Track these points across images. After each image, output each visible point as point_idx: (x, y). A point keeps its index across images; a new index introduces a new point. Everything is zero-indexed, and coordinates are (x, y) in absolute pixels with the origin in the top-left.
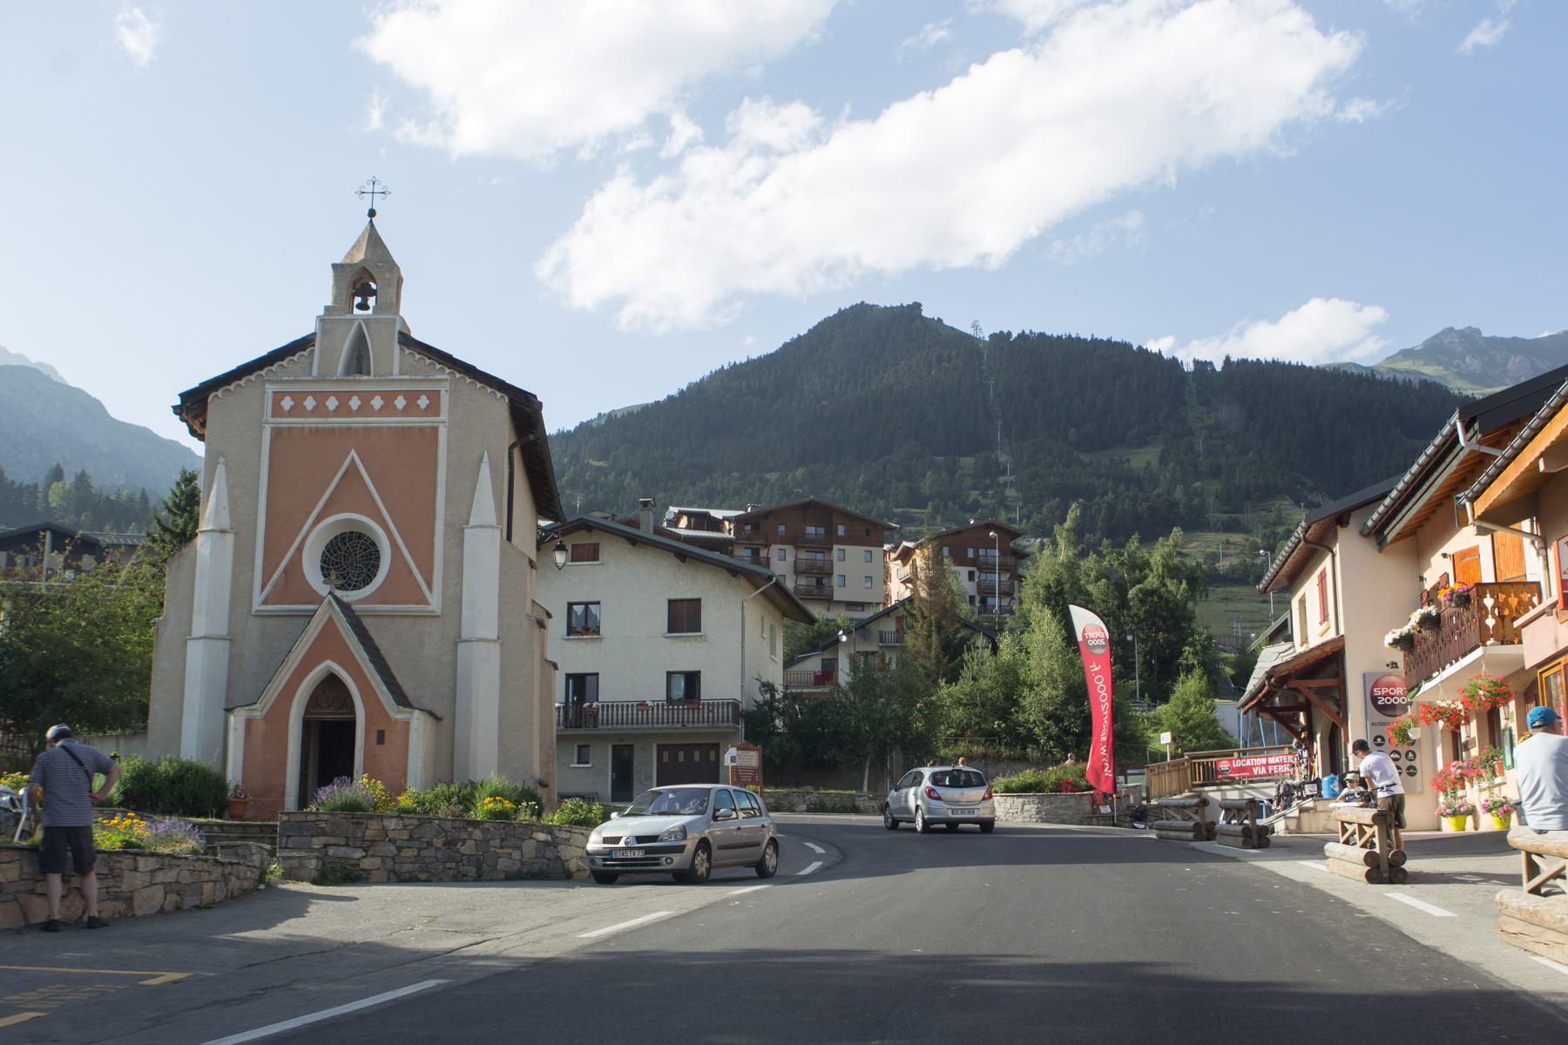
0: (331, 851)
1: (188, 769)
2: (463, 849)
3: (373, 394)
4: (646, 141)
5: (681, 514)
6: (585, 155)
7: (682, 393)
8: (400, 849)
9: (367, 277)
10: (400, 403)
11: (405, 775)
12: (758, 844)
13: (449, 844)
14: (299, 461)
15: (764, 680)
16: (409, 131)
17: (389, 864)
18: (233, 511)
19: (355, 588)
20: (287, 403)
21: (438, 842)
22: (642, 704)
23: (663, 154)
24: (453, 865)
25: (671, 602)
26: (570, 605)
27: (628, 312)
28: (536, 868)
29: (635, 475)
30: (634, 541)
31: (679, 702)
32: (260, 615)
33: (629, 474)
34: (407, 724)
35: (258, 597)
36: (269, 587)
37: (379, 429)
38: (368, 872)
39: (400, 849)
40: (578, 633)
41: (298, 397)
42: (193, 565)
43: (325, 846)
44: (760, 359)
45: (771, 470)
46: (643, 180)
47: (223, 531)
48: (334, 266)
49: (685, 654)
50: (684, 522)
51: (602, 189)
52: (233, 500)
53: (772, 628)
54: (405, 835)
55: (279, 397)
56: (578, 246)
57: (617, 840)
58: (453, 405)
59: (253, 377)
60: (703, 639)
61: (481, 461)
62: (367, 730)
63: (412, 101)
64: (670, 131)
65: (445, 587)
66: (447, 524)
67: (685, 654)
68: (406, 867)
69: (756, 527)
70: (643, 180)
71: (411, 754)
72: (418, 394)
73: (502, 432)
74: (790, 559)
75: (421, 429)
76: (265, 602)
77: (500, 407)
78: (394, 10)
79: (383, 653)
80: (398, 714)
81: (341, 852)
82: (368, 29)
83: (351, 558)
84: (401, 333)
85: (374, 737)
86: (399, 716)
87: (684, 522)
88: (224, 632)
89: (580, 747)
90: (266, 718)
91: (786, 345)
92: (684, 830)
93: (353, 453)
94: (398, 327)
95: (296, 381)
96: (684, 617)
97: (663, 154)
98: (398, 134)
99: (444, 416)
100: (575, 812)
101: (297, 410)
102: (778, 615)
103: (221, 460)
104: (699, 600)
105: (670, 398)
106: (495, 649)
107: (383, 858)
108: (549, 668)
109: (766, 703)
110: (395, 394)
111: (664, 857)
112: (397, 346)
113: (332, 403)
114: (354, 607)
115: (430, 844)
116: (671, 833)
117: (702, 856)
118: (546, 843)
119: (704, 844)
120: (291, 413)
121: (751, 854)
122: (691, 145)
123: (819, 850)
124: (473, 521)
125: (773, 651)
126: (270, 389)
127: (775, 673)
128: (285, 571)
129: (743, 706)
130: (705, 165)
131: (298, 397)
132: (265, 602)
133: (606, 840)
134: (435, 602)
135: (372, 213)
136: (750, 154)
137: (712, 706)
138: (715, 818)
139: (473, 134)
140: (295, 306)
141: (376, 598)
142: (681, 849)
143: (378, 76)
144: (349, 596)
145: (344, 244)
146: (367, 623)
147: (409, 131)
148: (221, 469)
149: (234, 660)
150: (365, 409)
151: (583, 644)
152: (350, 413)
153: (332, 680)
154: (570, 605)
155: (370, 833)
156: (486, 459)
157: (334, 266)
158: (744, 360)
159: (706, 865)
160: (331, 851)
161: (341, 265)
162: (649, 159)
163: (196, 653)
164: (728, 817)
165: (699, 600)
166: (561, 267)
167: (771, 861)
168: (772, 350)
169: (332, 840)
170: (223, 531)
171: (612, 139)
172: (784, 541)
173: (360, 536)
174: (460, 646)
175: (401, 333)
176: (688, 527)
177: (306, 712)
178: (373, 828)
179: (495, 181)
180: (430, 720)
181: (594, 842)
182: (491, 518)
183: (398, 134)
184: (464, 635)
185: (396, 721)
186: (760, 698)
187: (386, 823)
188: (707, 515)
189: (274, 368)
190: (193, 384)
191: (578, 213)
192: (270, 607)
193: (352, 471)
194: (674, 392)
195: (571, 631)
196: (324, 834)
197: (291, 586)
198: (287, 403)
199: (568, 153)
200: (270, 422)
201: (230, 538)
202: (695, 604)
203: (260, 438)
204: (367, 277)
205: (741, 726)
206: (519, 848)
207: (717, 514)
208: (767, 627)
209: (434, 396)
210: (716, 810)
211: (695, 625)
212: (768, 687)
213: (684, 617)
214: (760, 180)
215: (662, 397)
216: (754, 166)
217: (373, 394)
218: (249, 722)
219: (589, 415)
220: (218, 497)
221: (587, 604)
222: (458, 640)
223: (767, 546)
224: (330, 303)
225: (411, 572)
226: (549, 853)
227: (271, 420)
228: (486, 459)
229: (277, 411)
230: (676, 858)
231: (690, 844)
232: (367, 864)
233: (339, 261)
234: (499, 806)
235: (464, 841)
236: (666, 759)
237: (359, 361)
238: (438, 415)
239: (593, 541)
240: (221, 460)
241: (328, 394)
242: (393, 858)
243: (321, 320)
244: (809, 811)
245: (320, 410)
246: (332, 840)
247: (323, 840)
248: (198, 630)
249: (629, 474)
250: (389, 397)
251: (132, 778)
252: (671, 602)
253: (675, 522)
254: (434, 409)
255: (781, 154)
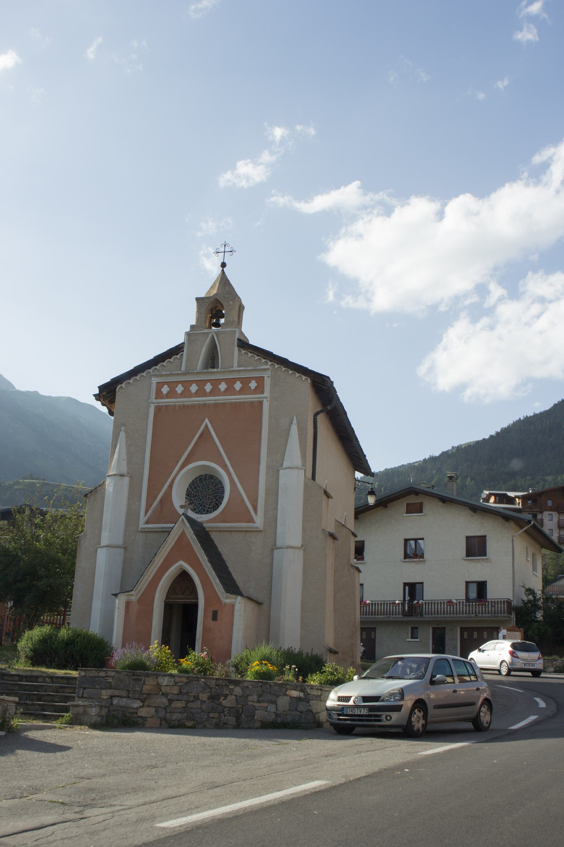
0: (115, 701)
1: (79, 635)
2: (225, 703)
3: (220, 381)
4: (475, 299)
5: (490, 495)
6: (442, 309)
7: (497, 433)
8: (170, 701)
9: (219, 307)
10: (238, 386)
11: (231, 642)
12: (473, 704)
13: (214, 698)
14: (172, 430)
15: (527, 587)
16: (349, 301)
17: (162, 713)
18: (129, 462)
19: (208, 512)
20: (165, 389)
21: (204, 697)
22: (450, 602)
23: (485, 306)
24: (216, 715)
25: (468, 538)
26: (406, 541)
27: (468, 392)
28: (289, 719)
29: (472, 479)
30: (444, 500)
31: (473, 600)
32: (144, 531)
33: (469, 479)
34: (233, 606)
35: (143, 519)
36: (150, 512)
37: (224, 404)
38: (144, 718)
39: (170, 701)
40: (411, 557)
41: (172, 385)
42: (103, 497)
43: (112, 697)
44: (541, 413)
45: (549, 475)
46: (474, 320)
47: (122, 475)
48: (198, 299)
49: (477, 570)
50: (492, 499)
51: (452, 326)
52: (130, 455)
53: (533, 555)
54: (176, 691)
55: (160, 385)
56: (440, 357)
57: (347, 699)
58: (273, 386)
59: (144, 374)
60: (488, 560)
61: (291, 423)
62: (205, 610)
63: (350, 285)
64: (489, 292)
65: (266, 511)
66: (268, 467)
67: (477, 570)
68: (176, 716)
69: (534, 501)
70: (474, 320)
71: (235, 628)
72: (250, 379)
73: (308, 401)
74: (555, 520)
75: (252, 403)
76: (147, 523)
77: (306, 384)
78: (339, 239)
79: (224, 557)
80: (227, 599)
81: (124, 702)
82: (326, 249)
83: (205, 492)
84: (239, 340)
85: (210, 615)
86: (228, 601)
87: (492, 499)
88: (120, 542)
89: (412, 628)
90: (139, 601)
91: (555, 405)
92: (402, 693)
93: (207, 420)
94: (237, 336)
95: (171, 375)
96: (476, 548)
97: (485, 306)
98: (343, 303)
99: (267, 393)
100: (332, 674)
101: (172, 394)
102: (538, 546)
103: (123, 428)
104: (485, 536)
105: (491, 436)
106: (300, 554)
107: (157, 709)
108: (353, 570)
109: (529, 601)
110: (234, 380)
111: (384, 714)
112: (236, 349)
113: (194, 388)
114: (205, 525)
115: (196, 698)
116: (391, 695)
117: (418, 714)
118: (299, 699)
119: (420, 704)
120: (168, 396)
121: (470, 711)
122: (501, 299)
123: (542, 704)
124: (285, 465)
125: (534, 569)
126: (155, 380)
127: (537, 585)
128: (161, 501)
129: (514, 603)
130: (508, 310)
131: (172, 385)
132: (147, 523)
133: (340, 699)
134: (259, 521)
135: (223, 265)
136: (533, 302)
137: (495, 603)
138: (432, 683)
139: (382, 301)
140: (173, 325)
141: (223, 518)
142: (398, 708)
143: (333, 274)
144: (201, 518)
145: (205, 287)
146: (214, 536)
147: (349, 301)
148: (122, 435)
149: (126, 563)
150: (215, 391)
151: (414, 564)
152: (205, 394)
153: (184, 576)
154: (406, 541)
155: (146, 688)
156: (295, 421)
157: (198, 299)
158: (532, 414)
159: (422, 722)
160: (115, 701)
161: (202, 298)
162: (476, 308)
163: (102, 556)
164: (443, 682)
165: (485, 536)
166: (431, 369)
167: (485, 717)
168: (548, 409)
169: (116, 692)
170: (122, 475)
171: (457, 299)
172: (551, 509)
173: (212, 477)
174: (275, 552)
175: (239, 340)
176: (495, 502)
177: (168, 597)
178: (149, 684)
179: (395, 325)
180: (251, 605)
181: (332, 701)
182: (298, 462)
183: (343, 303)
184: (278, 544)
185: (226, 604)
186: (525, 598)
187: (160, 680)
188: (505, 495)
189: (158, 367)
190: (107, 379)
191: (440, 339)
192: (150, 526)
193: (206, 433)
194: (493, 433)
195: (406, 556)
196: (111, 688)
197: (164, 512)
198: (165, 389)
199: (433, 308)
200: (154, 402)
201: (126, 480)
202: (482, 539)
203: (147, 415)
204: (219, 307)
205: (513, 616)
206: (274, 702)
207: (512, 494)
208: (530, 554)
209: (260, 381)
210: (433, 676)
211: (482, 552)
212: (530, 591)
213: (476, 548)
214: (538, 316)
215: (487, 437)
216: (536, 309)
217: (220, 381)
218: (128, 604)
219: (447, 447)
220: (119, 452)
221: (416, 540)
222: (274, 547)
223: (541, 512)
224: (194, 323)
225: (243, 501)
226: (302, 707)
227: (154, 401)
228: (295, 421)
229: (159, 395)
230: (395, 716)
231: (408, 703)
232: (143, 712)
233: (202, 295)
234: (264, 668)
235: (226, 696)
236: (466, 636)
237: (212, 360)
238: (263, 393)
239: (419, 501)
240: (123, 428)
241: (191, 382)
242: (165, 708)
243: (188, 334)
244: (556, 672)
245: (186, 393)
246: (116, 692)
247: (110, 692)
248: (105, 541)
249: (469, 479)
250: (230, 382)
251: (40, 641)
252: (468, 538)
253: (487, 499)
254: (260, 389)
255: (551, 301)
